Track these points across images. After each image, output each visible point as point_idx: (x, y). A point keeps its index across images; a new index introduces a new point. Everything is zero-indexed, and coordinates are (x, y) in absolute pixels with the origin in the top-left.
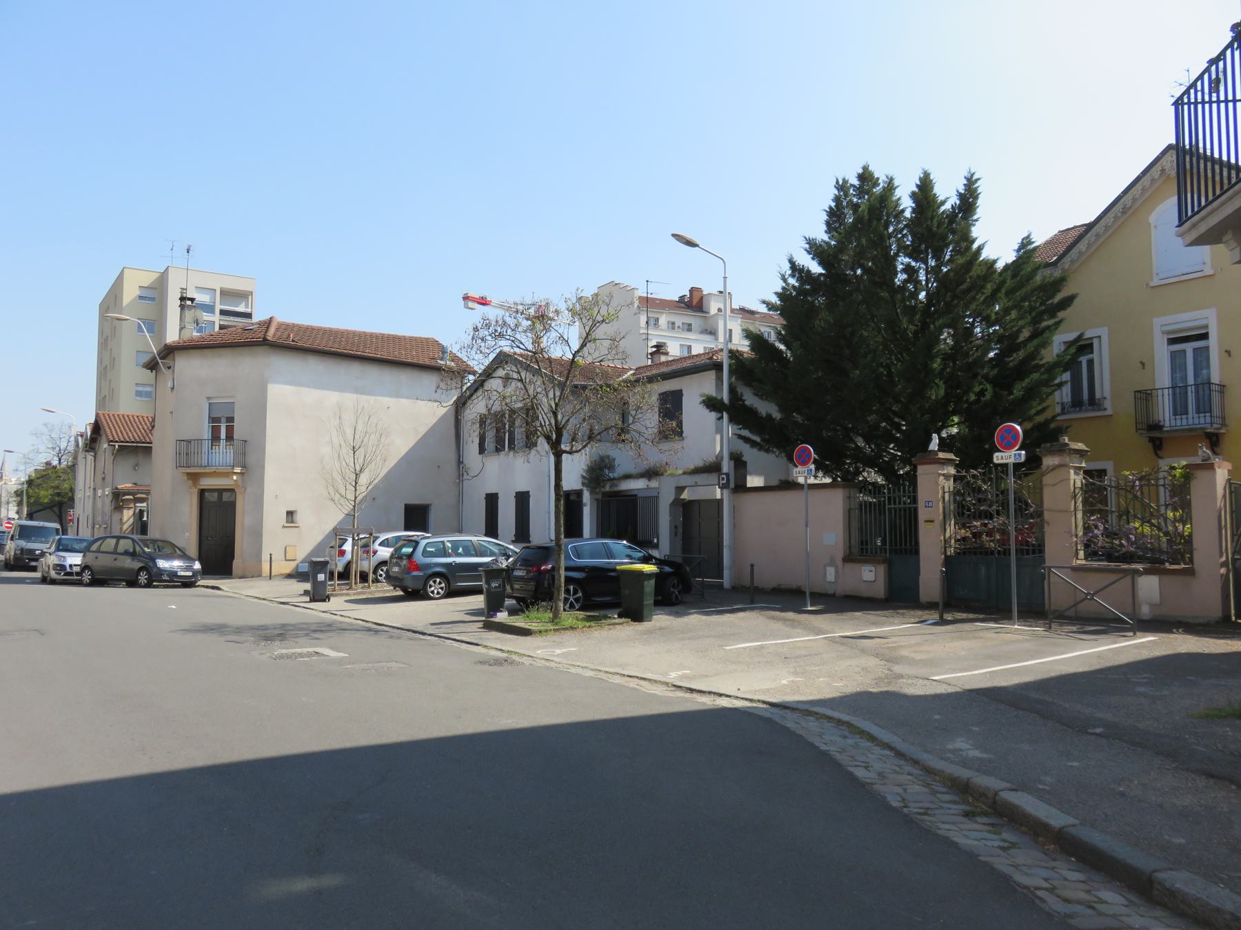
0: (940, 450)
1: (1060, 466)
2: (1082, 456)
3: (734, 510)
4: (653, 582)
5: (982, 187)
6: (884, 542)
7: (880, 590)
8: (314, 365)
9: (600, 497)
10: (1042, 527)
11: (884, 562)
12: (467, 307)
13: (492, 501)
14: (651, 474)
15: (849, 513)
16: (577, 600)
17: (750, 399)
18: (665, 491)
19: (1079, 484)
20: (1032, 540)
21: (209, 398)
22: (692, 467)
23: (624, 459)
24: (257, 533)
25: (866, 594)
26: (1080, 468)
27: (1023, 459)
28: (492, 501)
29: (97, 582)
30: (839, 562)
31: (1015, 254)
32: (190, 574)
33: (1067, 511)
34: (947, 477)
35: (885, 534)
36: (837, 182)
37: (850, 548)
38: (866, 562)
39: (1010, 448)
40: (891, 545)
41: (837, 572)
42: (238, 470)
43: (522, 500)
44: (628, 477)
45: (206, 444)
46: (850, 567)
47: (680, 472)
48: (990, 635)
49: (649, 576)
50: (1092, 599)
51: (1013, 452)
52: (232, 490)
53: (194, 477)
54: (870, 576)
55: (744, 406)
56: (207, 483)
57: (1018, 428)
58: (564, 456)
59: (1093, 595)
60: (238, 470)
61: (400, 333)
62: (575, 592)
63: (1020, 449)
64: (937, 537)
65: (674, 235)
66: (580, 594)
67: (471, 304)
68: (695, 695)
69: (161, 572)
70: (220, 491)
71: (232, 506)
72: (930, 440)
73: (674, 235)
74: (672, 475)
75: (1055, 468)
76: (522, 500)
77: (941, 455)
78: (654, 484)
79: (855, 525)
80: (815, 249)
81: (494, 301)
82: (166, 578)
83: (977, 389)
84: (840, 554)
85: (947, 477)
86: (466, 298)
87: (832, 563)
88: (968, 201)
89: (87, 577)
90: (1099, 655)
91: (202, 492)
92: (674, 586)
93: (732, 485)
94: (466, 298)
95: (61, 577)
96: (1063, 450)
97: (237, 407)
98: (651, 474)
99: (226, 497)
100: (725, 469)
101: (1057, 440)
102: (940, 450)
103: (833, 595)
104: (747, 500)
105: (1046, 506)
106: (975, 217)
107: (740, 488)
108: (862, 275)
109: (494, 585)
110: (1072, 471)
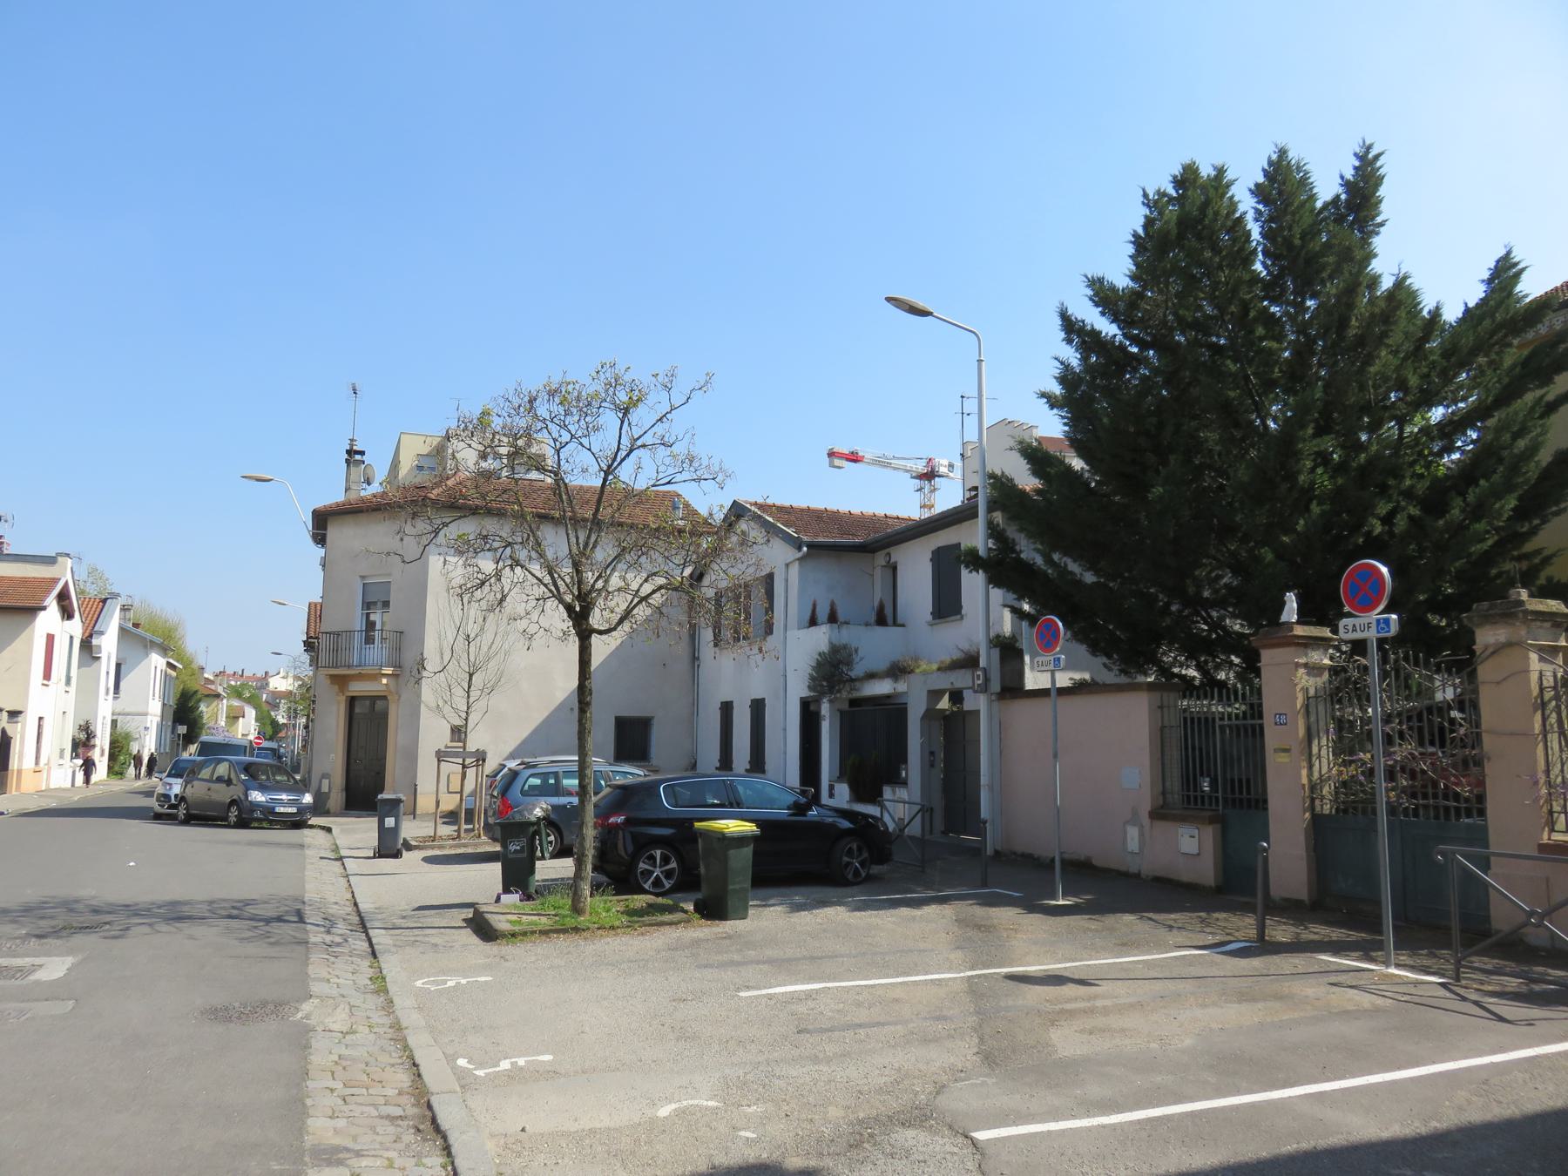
0: (1298, 622)
1: (1509, 645)
2: (1557, 625)
3: (1001, 730)
4: (748, 851)
5: (1387, 166)
6: (1214, 784)
7: (1206, 872)
8: (349, 518)
9: (845, 706)
10: (1479, 763)
11: (1211, 821)
12: (832, 465)
13: (727, 708)
14: (897, 671)
15: (1161, 735)
16: (668, 875)
17: (1029, 551)
18: (915, 695)
19: (1549, 681)
20: (1465, 791)
21: (363, 577)
22: (947, 660)
23: (873, 647)
24: (412, 757)
25: (1186, 877)
26: (1554, 650)
27: (1394, 629)
28: (727, 708)
29: (192, 819)
30: (1146, 821)
31: (1483, 287)
32: (294, 810)
33: (1527, 734)
34: (1314, 670)
35: (1214, 774)
36: (1145, 195)
37: (1164, 793)
38: (1183, 819)
39: (1369, 608)
40: (1225, 791)
41: (1141, 835)
42: (389, 671)
43: (758, 707)
44: (871, 676)
45: (358, 639)
46: (1163, 827)
47: (935, 667)
48: (1311, 990)
49: (741, 840)
50: (1540, 925)
51: (1375, 615)
52: (385, 698)
53: (340, 681)
54: (1190, 847)
55: (1019, 561)
56: (357, 688)
57: (1384, 570)
58: (595, 639)
59: (1542, 917)
60: (389, 671)
61: (832, 506)
62: (665, 860)
63: (1387, 610)
64: (1300, 773)
65: (889, 299)
66: (673, 865)
67: (837, 462)
68: (1069, 990)
69: (255, 806)
70: (374, 699)
71: (384, 716)
72: (1281, 605)
73: (889, 299)
74: (925, 673)
75: (1499, 649)
76: (758, 707)
77: (1300, 631)
78: (901, 687)
79: (1175, 754)
80: (1103, 295)
81: (868, 456)
82: (258, 814)
83: (1383, 508)
84: (1146, 807)
85: (1314, 670)
86: (831, 454)
87: (1134, 819)
88: (1362, 193)
89: (182, 812)
90: (1483, 1080)
91: (352, 701)
92: (850, 852)
93: (996, 686)
94: (831, 454)
95: (165, 810)
96: (1512, 612)
97: (393, 587)
98: (897, 671)
99: (379, 705)
100: (982, 663)
101: (1505, 597)
102: (1298, 622)
103: (1137, 876)
104: (1020, 708)
105: (1484, 726)
106: (1379, 220)
107: (1012, 689)
108: (1479, 430)
109: (512, 848)
110: (1534, 657)
